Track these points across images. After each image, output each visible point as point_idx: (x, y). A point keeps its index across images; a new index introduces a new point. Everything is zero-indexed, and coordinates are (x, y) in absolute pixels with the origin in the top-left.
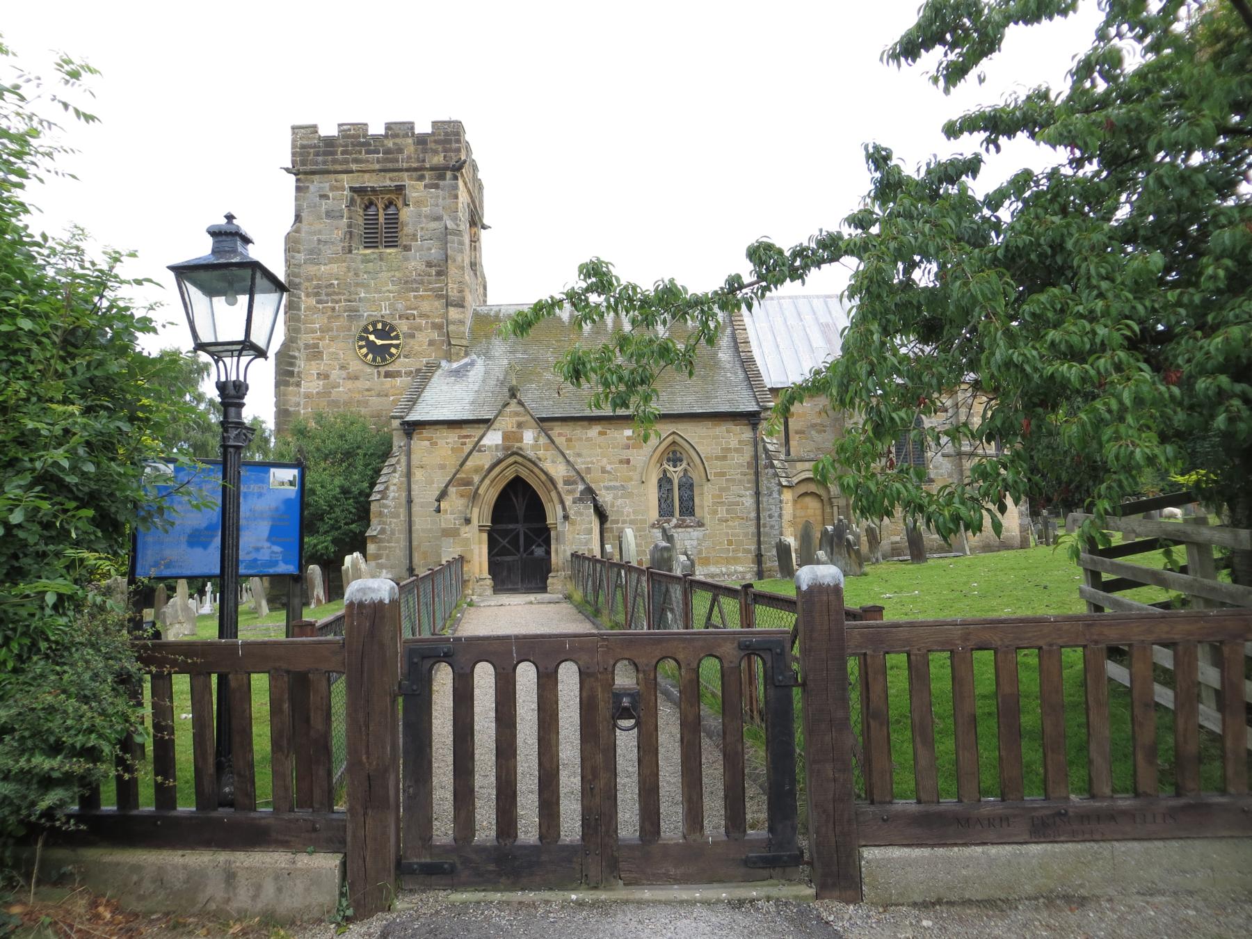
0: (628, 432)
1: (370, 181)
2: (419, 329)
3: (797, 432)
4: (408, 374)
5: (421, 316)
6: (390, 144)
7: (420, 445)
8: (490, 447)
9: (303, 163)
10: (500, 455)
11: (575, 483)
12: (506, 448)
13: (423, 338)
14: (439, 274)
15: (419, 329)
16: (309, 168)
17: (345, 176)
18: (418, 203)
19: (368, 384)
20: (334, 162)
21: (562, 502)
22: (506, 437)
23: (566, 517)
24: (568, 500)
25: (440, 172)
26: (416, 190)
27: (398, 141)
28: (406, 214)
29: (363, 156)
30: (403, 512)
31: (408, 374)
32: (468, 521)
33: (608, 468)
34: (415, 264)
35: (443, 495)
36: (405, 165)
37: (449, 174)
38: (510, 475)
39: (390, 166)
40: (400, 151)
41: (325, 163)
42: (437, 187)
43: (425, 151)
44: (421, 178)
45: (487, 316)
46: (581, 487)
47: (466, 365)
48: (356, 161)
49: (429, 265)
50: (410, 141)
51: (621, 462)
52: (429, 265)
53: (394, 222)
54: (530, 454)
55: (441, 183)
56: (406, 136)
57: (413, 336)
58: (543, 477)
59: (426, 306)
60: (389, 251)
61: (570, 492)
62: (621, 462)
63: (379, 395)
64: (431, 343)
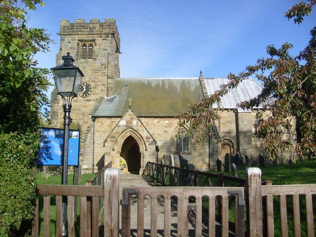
0: (167, 122)
1: (84, 37)
2: (98, 85)
3: (223, 124)
4: (94, 100)
5: (99, 81)
6: (91, 26)
7: (98, 122)
8: (122, 126)
9: (64, 32)
10: (125, 128)
11: (149, 138)
12: (127, 126)
13: (99, 89)
14: (105, 68)
15: (98, 85)
16: (66, 33)
17: (76, 36)
18: (100, 45)
19: (80, 103)
20: (73, 32)
21: (145, 145)
22: (127, 122)
23: (146, 150)
24: (147, 144)
25: (107, 35)
26: (99, 40)
27: (94, 25)
28: (96, 48)
29: (83, 30)
30: (92, 146)
31: (94, 100)
32: (113, 150)
33: (160, 134)
34: (97, 64)
35: (106, 141)
36: (96, 33)
37: (110, 36)
38: (128, 135)
39: (91, 33)
40: (95, 28)
41: (70, 32)
42: (106, 40)
43: (103, 28)
44: (101, 37)
45: (120, 82)
46: (152, 140)
47: (113, 98)
48: (81, 31)
49: (102, 65)
50: (98, 25)
51: (164, 132)
52: (102, 65)
53: (91, 51)
54: (135, 128)
55: (107, 38)
56: (97, 23)
57: (96, 88)
58: (139, 136)
59: (100, 78)
60: (89, 60)
61: (149, 141)
62: (164, 132)
63: (84, 107)
64: (102, 90)
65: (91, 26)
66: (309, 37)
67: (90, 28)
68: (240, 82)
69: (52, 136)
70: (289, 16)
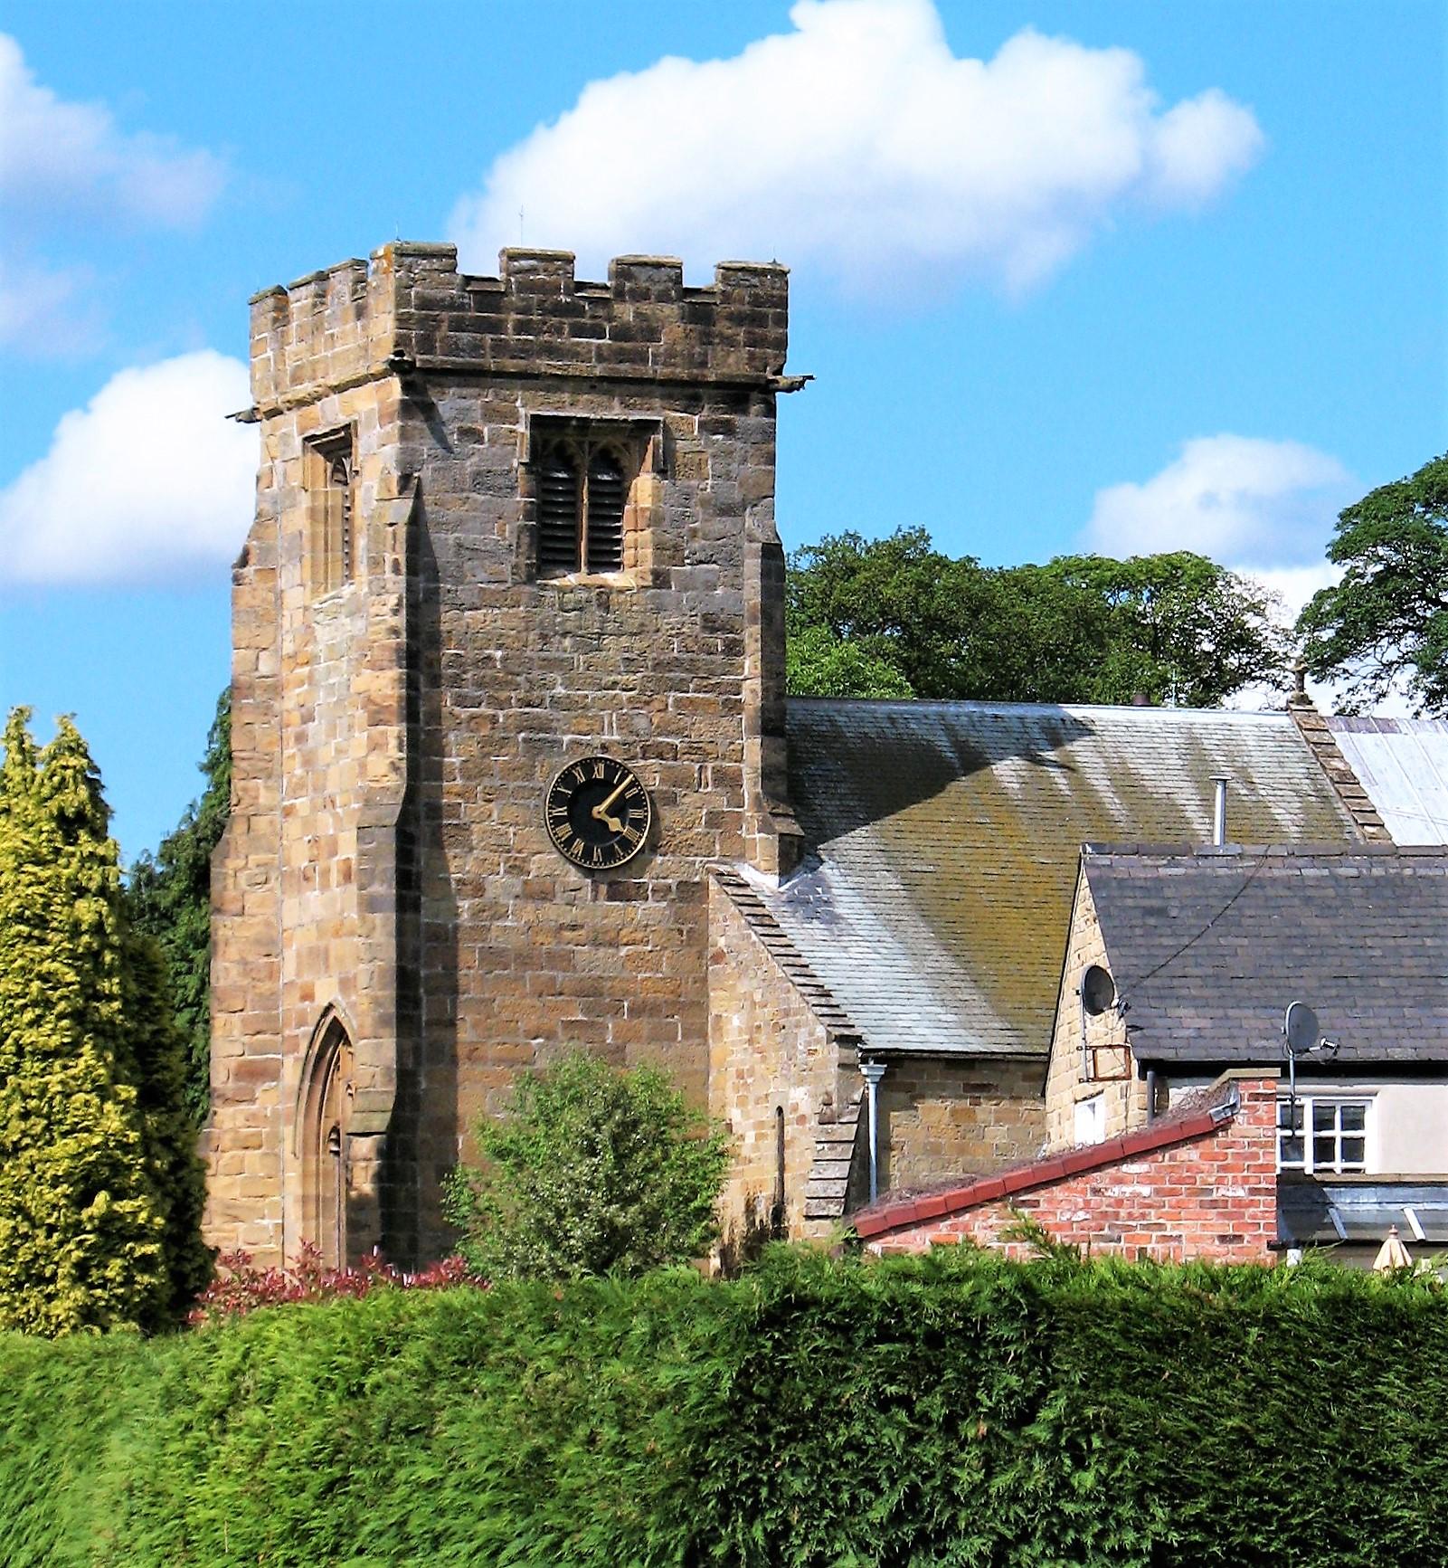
5: (693, 749)
6: (626, 312)
9: (427, 345)
20: (500, 348)
27: (646, 308)
36: (662, 372)
39: (625, 368)
40: (652, 334)
41: (476, 348)
48: (551, 351)
63: (597, 944)
65: (626, 312)
66: (73, 432)
67: (621, 334)
68: (199, 801)
69: (1044, 1136)
70: (719, 267)
